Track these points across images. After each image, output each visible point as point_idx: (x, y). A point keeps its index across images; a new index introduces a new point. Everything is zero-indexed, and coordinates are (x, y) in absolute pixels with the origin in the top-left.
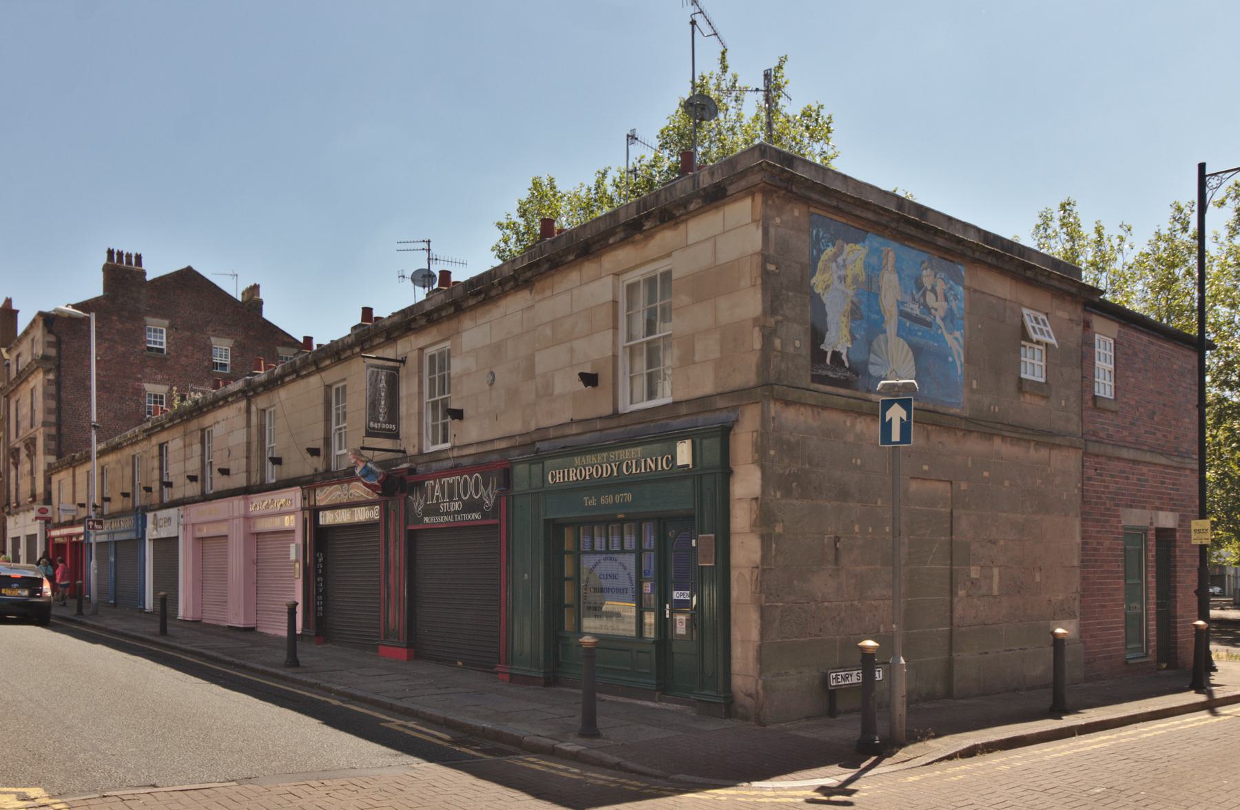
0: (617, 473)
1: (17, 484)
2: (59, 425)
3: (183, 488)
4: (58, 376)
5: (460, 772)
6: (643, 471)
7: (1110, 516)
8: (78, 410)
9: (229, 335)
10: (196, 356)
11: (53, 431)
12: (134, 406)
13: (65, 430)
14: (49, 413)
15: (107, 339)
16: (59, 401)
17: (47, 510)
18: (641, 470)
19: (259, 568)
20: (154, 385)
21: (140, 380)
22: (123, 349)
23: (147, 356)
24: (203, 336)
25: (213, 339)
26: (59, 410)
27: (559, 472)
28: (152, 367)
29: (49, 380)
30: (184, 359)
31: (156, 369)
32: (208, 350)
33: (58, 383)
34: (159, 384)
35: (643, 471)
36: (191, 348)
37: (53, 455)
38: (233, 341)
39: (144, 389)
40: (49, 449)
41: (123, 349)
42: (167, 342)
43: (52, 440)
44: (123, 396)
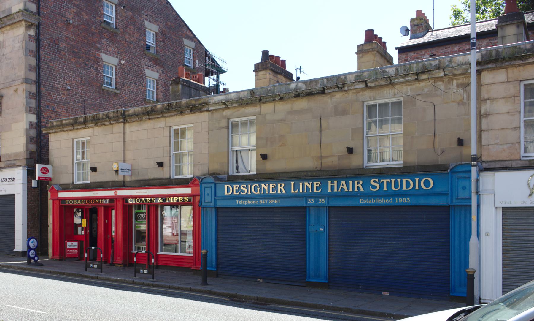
0: (263, 192)
1: (170, 146)
2: (38, 83)
3: (322, 155)
4: (38, 34)
5: (429, 41)
6: (301, 191)
7: (67, 11)
8: (54, 70)
9: (156, 21)
10: (135, 36)
11: (34, 89)
12: (95, 73)
13: (43, 90)
14: (30, 70)
15: (75, 5)
16: (39, 60)
17: (48, 170)
18: (299, 190)
19: (396, 152)
20: (108, 56)
21: (98, 50)
22: (87, 17)
23: (104, 28)
24: (140, 18)
25: (146, 22)
26: (38, 68)
27: (75, 203)
28: (107, 39)
29: (30, 36)
30: (128, 36)
31: (110, 42)
32: (142, 31)
33: (38, 39)
34: (111, 55)
35: (301, 191)
36: (132, 27)
37: (33, 113)
38: (158, 27)
39: (102, 59)
40: (30, 107)
41: (87, 17)
42: (116, 19)
43: (32, 99)
44: (87, 63)
